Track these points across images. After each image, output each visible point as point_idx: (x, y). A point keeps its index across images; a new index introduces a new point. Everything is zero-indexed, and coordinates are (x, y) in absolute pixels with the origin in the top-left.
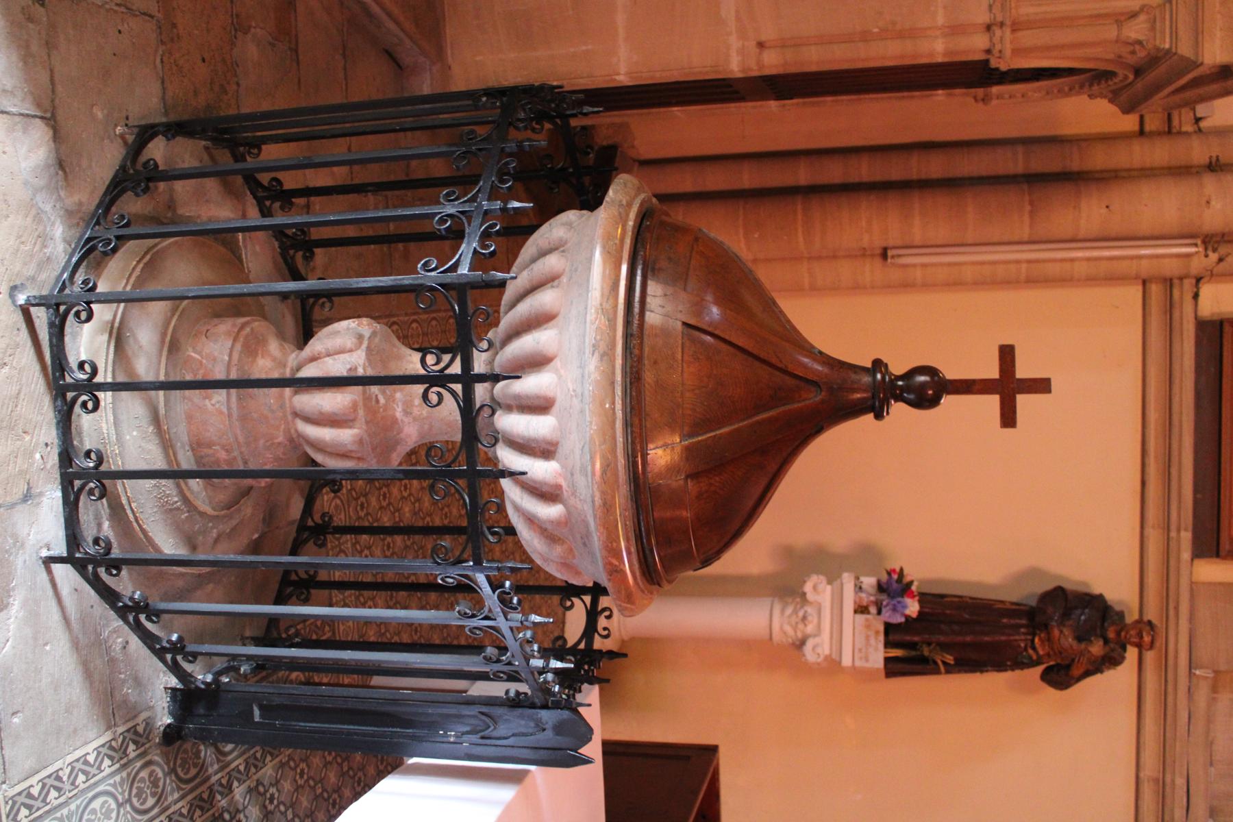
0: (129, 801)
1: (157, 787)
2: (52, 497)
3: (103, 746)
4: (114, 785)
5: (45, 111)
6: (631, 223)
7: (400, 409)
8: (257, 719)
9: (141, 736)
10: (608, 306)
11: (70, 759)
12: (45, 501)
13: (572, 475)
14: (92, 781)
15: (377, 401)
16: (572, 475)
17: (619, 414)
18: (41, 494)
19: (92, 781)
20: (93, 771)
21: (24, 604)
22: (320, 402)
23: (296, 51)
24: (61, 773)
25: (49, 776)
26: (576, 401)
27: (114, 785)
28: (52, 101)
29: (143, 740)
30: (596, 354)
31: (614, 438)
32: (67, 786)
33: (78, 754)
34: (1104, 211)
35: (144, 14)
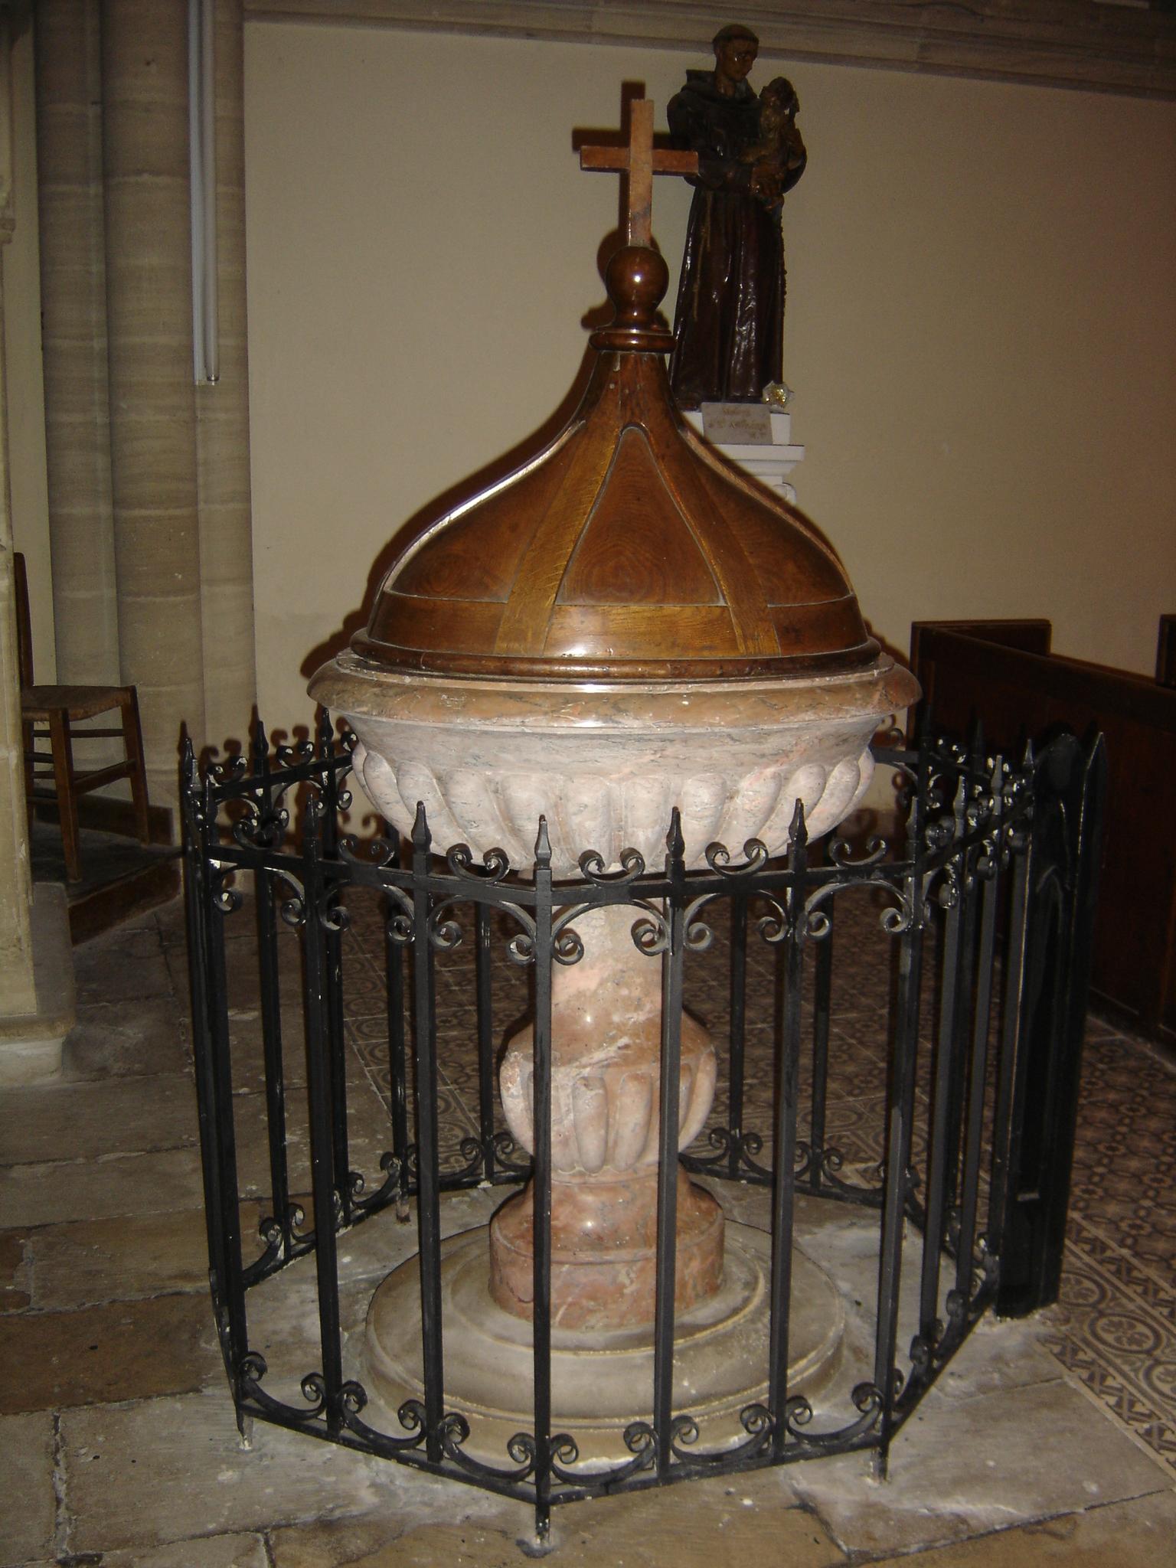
0: (1149, 1352)
1: (1120, 1324)
2: (802, 1477)
3: (1092, 1389)
4: (1136, 1371)
5: (257, 1541)
6: (407, 680)
7: (635, 1015)
8: (1034, 1196)
9: (1064, 1347)
10: (546, 706)
11: (1119, 1424)
12: (803, 1485)
13: (763, 756)
14: (1138, 1395)
15: (626, 1047)
16: (763, 756)
17: (692, 688)
18: (796, 1493)
19: (1138, 1395)
20: (1126, 1397)
21: (945, 1494)
22: (631, 1126)
23: (30, 1229)
24: (1141, 1431)
25: (1150, 1443)
26: (670, 750)
27: (1136, 1371)
28: (237, 1532)
29: (1069, 1345)
30: (617, 718)
31: (727, 694)
32: (1155, 1423)
33: (1110, 1415)
34: (153, 68)
35: (56, 1428)
